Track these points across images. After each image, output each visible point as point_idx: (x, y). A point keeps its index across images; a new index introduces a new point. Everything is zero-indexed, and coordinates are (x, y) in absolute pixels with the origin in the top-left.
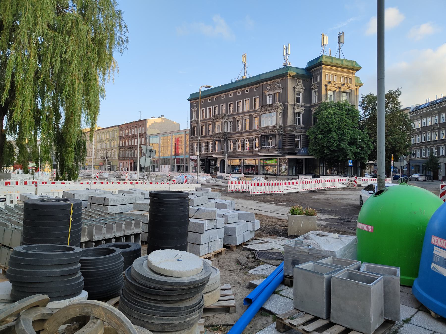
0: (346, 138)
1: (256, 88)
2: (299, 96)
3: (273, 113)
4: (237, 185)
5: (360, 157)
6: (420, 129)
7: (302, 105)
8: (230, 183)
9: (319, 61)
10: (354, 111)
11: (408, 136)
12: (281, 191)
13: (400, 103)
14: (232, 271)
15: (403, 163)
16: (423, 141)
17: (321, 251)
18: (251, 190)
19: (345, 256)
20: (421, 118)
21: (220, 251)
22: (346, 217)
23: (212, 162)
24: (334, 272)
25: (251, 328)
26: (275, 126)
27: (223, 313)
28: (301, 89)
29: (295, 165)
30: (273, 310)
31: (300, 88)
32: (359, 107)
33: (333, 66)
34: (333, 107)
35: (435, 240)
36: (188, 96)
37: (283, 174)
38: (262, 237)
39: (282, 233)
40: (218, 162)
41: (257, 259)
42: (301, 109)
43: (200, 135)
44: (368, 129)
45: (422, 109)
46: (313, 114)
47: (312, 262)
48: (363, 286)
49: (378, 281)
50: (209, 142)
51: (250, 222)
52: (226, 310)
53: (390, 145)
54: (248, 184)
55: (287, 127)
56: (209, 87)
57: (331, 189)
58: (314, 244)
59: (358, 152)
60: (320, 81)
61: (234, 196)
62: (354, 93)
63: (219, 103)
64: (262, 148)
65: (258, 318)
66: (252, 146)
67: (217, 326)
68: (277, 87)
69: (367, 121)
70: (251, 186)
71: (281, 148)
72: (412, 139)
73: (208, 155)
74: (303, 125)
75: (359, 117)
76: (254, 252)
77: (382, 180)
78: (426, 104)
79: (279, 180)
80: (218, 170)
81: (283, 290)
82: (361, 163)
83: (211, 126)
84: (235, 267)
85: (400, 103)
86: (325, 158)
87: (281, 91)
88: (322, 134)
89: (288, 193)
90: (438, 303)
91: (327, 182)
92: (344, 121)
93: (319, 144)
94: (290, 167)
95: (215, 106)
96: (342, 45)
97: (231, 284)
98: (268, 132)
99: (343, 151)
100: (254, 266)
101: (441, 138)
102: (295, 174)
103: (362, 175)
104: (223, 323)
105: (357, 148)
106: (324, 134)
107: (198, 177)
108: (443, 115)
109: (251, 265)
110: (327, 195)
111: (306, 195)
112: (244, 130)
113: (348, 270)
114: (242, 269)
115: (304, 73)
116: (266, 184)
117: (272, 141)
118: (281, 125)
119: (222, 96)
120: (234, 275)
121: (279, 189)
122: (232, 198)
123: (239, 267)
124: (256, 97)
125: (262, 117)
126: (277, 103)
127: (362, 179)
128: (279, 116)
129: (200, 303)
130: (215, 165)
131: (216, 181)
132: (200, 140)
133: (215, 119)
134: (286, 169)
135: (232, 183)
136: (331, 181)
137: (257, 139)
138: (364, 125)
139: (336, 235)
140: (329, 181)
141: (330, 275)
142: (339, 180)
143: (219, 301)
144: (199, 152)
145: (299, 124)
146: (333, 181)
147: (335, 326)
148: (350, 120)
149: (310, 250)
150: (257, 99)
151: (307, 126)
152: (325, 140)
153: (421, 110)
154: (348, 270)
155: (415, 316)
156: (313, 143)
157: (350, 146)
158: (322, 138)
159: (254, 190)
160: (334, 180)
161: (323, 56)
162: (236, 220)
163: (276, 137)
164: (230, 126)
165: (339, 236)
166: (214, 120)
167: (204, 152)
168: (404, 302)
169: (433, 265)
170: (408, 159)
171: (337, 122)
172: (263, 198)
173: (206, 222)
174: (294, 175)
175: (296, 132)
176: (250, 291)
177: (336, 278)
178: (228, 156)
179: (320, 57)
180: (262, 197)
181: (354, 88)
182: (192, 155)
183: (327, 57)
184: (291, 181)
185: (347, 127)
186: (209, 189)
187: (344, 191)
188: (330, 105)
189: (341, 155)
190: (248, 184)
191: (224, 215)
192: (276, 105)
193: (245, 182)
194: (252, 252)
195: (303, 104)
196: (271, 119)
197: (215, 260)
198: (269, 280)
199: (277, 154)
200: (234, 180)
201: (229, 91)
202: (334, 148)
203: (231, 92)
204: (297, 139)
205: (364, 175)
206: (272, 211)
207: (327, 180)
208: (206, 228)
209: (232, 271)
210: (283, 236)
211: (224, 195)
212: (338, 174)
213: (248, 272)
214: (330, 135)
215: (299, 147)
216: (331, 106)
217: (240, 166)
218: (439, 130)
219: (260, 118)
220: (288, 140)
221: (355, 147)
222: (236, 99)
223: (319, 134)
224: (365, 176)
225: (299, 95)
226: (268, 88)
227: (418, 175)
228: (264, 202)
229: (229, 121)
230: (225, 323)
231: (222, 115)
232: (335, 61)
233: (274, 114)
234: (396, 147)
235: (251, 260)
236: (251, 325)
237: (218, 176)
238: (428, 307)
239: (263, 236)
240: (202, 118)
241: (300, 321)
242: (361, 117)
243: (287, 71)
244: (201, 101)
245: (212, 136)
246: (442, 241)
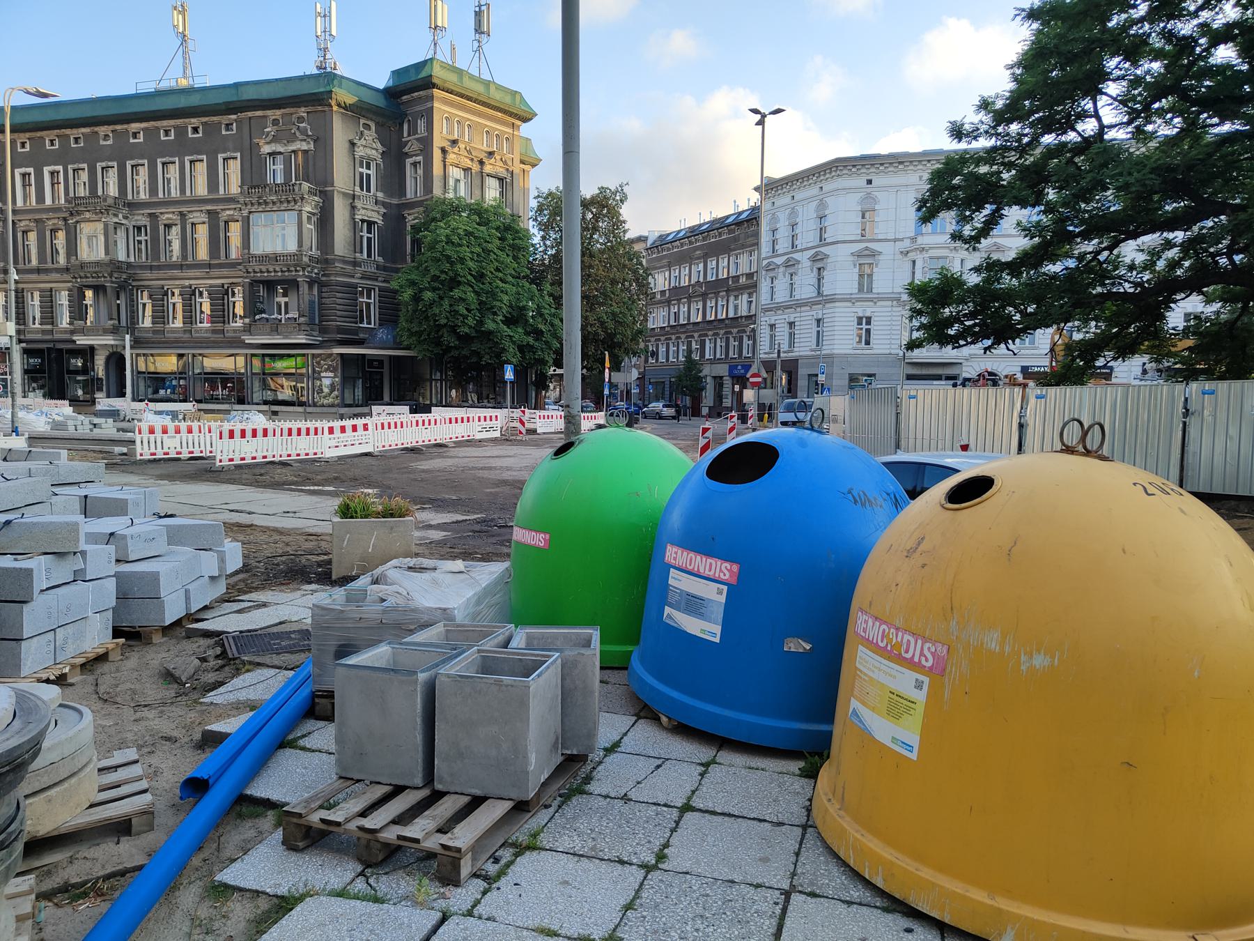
0: (498, 304)
1: (227, 125)
2: (368, 172)
3: (289, 212)
4: (168, 437)
5: (535, 358)
6: (667, 292)
7: (376, 200)
8: (145, 429)
9: (423, 74)
10: (517, 232)
11: (642, 309)
12: (319, 451)
13: (624, 222)
14: (146, 706)
15: (630, 375)
16: (672, 323)
17: (415, 610)
18: (219, 452)
19: (479, 617)
20: (669, 266)
21: (101, 651)
22: (496, 516)
23: (73, 361)
24: (443, 662)
25: (205, 860)
26: (297, 256)
27: (108, 840)
28: (374, 151)
29: (361, 375)
30: (275, 796)
31: (370, 146)
32: (531, 220)
33: (462, 96)
34: (463, 214)
35: (673, 554)
37: (326, 402)
38: (251, 592)
39: (315, 574)
40: (97, 362)
41: (230, 659)
42: (373, 211)
43: (16, 262)
44: (552, 285)
45: (671, 242)
46: (409, 228)
47: (389, 643)
48: (512, 686)
49: (548, 667)
50: (59, 290)
51: (210, 549)
52: (122, 828)
53: (602, 328)
54: (210, 432)
56: (45, 96)
57: (459, 444)
58: (398, 595)
59: (528, 344)
60: (426, 134)
61: (158, 472)
62: (518, 183)
63: (92, 156)
64: (255, 321)
65: (228, 828)
66: (221, 313)
67: (85, 883)
68: (298, 134)
69: (549, 262)
70: (221, 438)
71: (317, 322)
72: (650, 320)
73: (57, 336)
74: (381, 259)
75: (531, 249)
76: (222, 639)
77: (573, 417)
78: (679, 232)
79: (301, 421)
80: (100, 389)
81: (310, 733)
82: (536, 372)
83: (61, 235)
84: (154, 691)
85: (624, 222)
86: (446, 357)
87: (312, 146)
88: (434, 289)
89: (340, 458)
90: (675, 694)
91: (450, 422)
92: (492, 256)
93: (427, 318)
94: (347, 380)
95: (75, 166)
96: (486, 40)
97: (139, 747)
99: (490, 340)
100: (221, 680)
101: (708, 318)
102: (360, 402)
103: (539, 406)
104: (108, 871)
105: (527, 334)
106: (439, 289)
107: (17, 410)
108: (711, 261)
109: (211, 677)
110: (449, 460)
111: (392, 461)
112: (190, 259)
113: (479, 651)
114: (181, 695)
115: (380, 102)
116: (270, 433)
117: (286, 299)
118: (315, 252)
120: (151, 716)
121: (311, 445)
122: (153, 481)
123: (170, 691)
124: (228, 154)
125: (251, 224)
126: (300, 184)
127: (538, 414)
129: (10, 830)
130: (84, 371)
131: (92, 427)
132: (16, 282)
133: (78, 213)
135: (152, 431)
136: (459, 420)
137: (236, 291)
138: (543, 271)
139: (459, 565)
140: (453, 421)
141: (432, 672)
142: (482, 419)
143: (91, 806)
144: (17, 323)
145: (369, 255)
146: (465, 420)
147: (445, 798)
148: (508, 255)
149: (385, 612)
150: (231, 162)
151: (394, 262)
152: (442, 305)
153: (669, 245)
154: (479, 651)
155: (629, 734)
156: (410, 313)
157: (508, 327)
158: (434, 301)
159: (231, 453)
160: (468, 418)
161: (435, 62)
162: (161, 546)
163: (301, 289)
164: (140, 242)
165: (466, 567)
166: (72, 214)
167: (37, 326)
168: (611, 706)
169: (667, 610)
170: (642, 364)
171: (475, 258)
172: (261, 475)
173: (39, 564)
174: (357, 406)
175: (361, 278)
176: (208, 754)
177: (448, 676)
178: (136, 343)
179: (425, 62)
180: (257, 471)
181: (517, 168)
183: (445, 66)
184: (348, 423)
185: (500, 275)
186: (60, 453)
187: (494, 448)
188: (456, 208)
189: (487, 351)
190: (210, 432)
191: (112, 534)
192: (296, 188)
193: (200, 427)
194: (217, 639)
195: (380, 195)
196: (283, 232)
197: (84, 682)
198: (266, 713)
199: (304, 341)
200: (159, 422)
201: (128, 122)
202: (467, 330)
203: (135, 126)
204: (365, 300)
205: (545, 404)
206: (288, 512)
207: (450, 419)
208: (40, 582)
209: (146, 706)
210: (318, 582)
211: (123, 471)
212: (478, 402)
213: (202, 700)
214: (456, 293)
215: (370, 324)
216: (459, 212)
217: (181, 374)
218: (704, 297)
219: (246, 225)
220: (336, 301)
221: (520, 330)
222: (154, 152)
223: (426, 289)
224: (546, 406)
225: (368, 167)
226: (268, 133)
227: (661, 405)
228: (265, 487)
229: (134, 223)
230: (114, 869)
231: (105, 200)
232: (467, 83)
233: (290, 218)
234: (615, 335)
235: (213, 663)
236: (205, 854)
237: (98, 407)
238: (655, 707)
239: (256, 589)
240: (25, 202)
241: (354, 807)
242: (537, 249)
243: (328, 89)
244: (13, 142)
245: (67, 270)
246: (685, 554)
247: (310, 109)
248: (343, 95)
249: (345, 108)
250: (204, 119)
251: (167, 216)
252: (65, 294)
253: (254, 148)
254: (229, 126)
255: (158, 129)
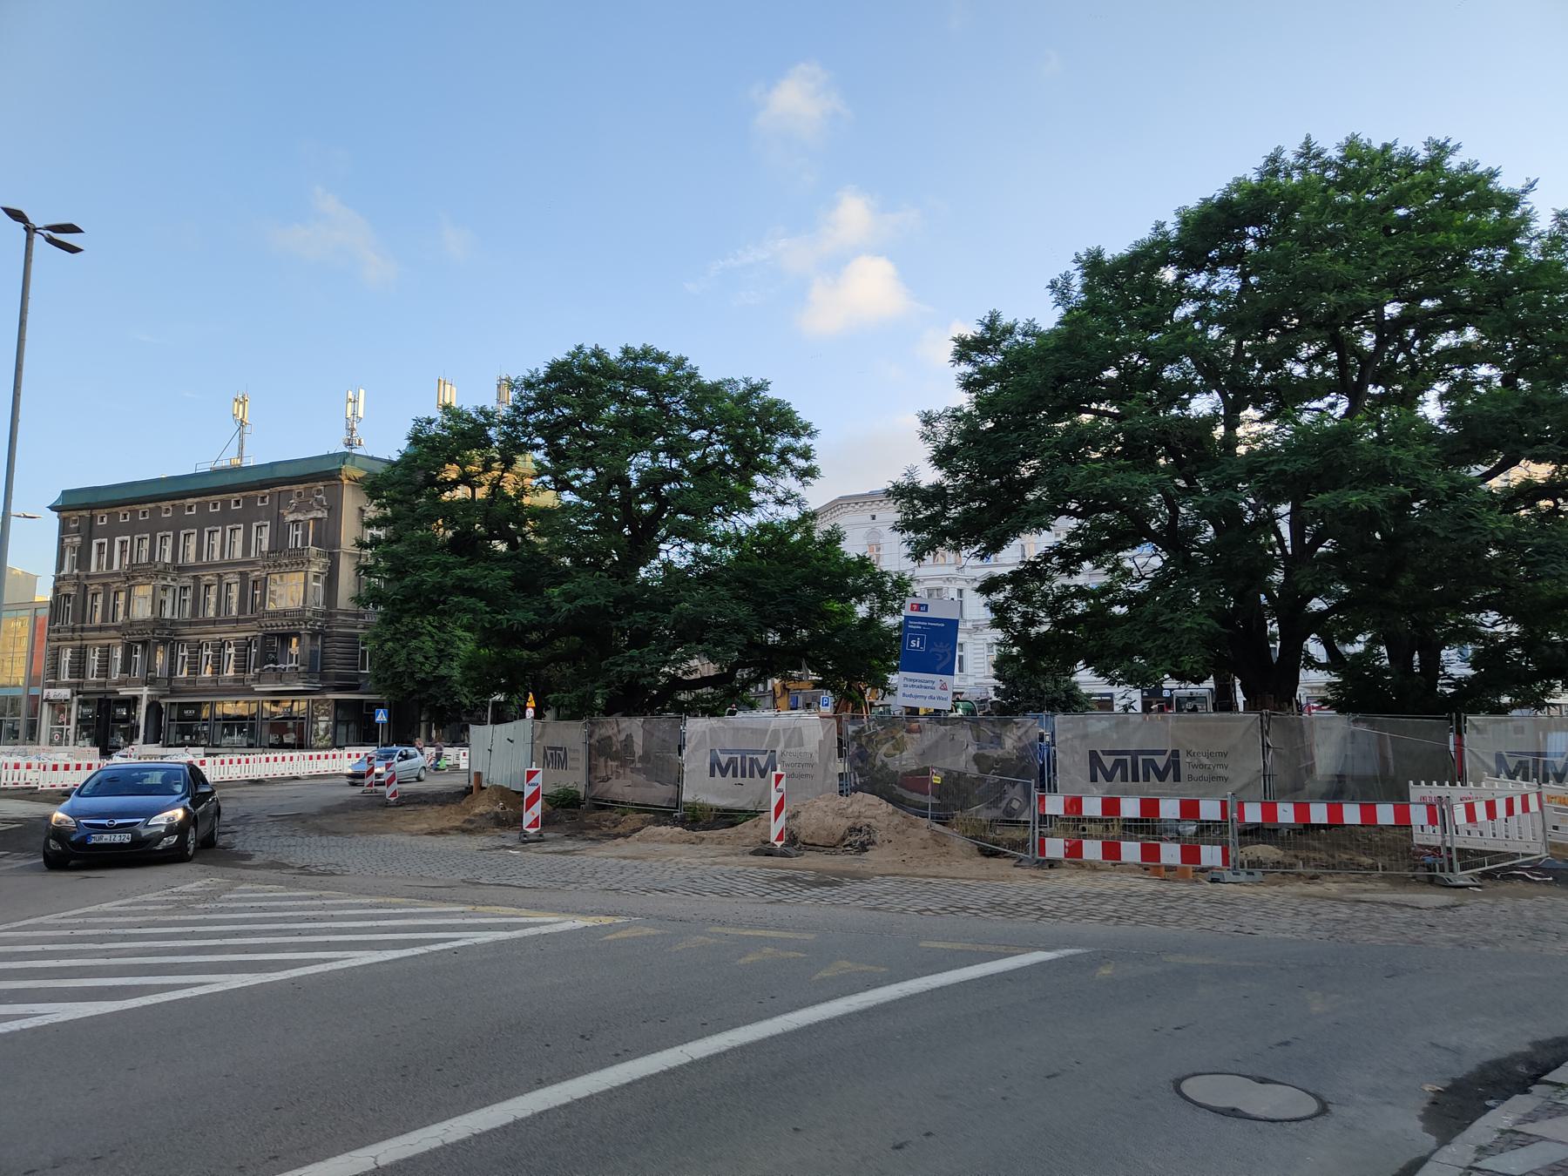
0: (455, 651)
23: (118, 710)
26: (301, 611)
36: (54, 497)
37: (320, 744)
50: (116, 646)
55: (336, 614)
63: (153, 527)
87: (326, 515)
95: (140, 536)
98: (282, 626)
118: (321, 607)
119: (164, 508)
128: (314, 584)
133: (134, 578)
134: (327, 730)
167: (95, 678)
182: (51, 686)
199: (302, 688)
201: (185, 498)
202: (423, 675)
203: (190, 501)
220: (337, 650)
222: (203, 522)
229: (181, 585)
247: (326, 483)
248: (351, 471)
249: (356, 481)
250: (244, 494)
251: (208, 577)
252: (119, 649)
253: (280, 517)
254: (263, 502)
255: (208, 503)
